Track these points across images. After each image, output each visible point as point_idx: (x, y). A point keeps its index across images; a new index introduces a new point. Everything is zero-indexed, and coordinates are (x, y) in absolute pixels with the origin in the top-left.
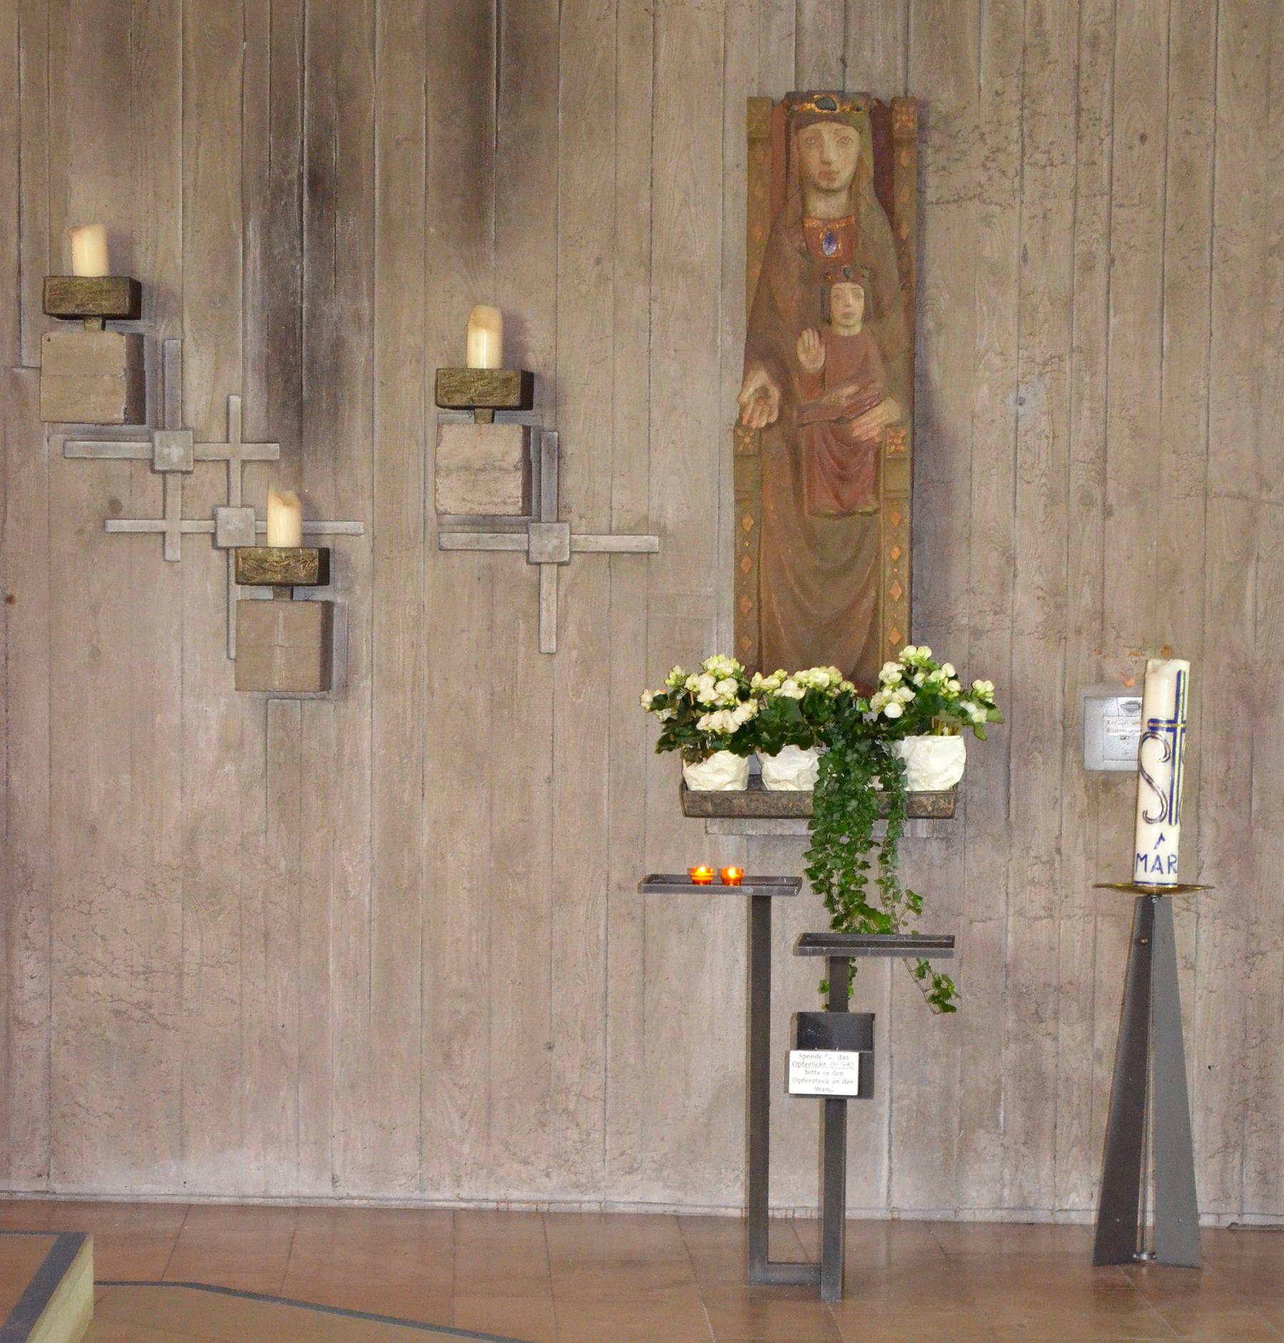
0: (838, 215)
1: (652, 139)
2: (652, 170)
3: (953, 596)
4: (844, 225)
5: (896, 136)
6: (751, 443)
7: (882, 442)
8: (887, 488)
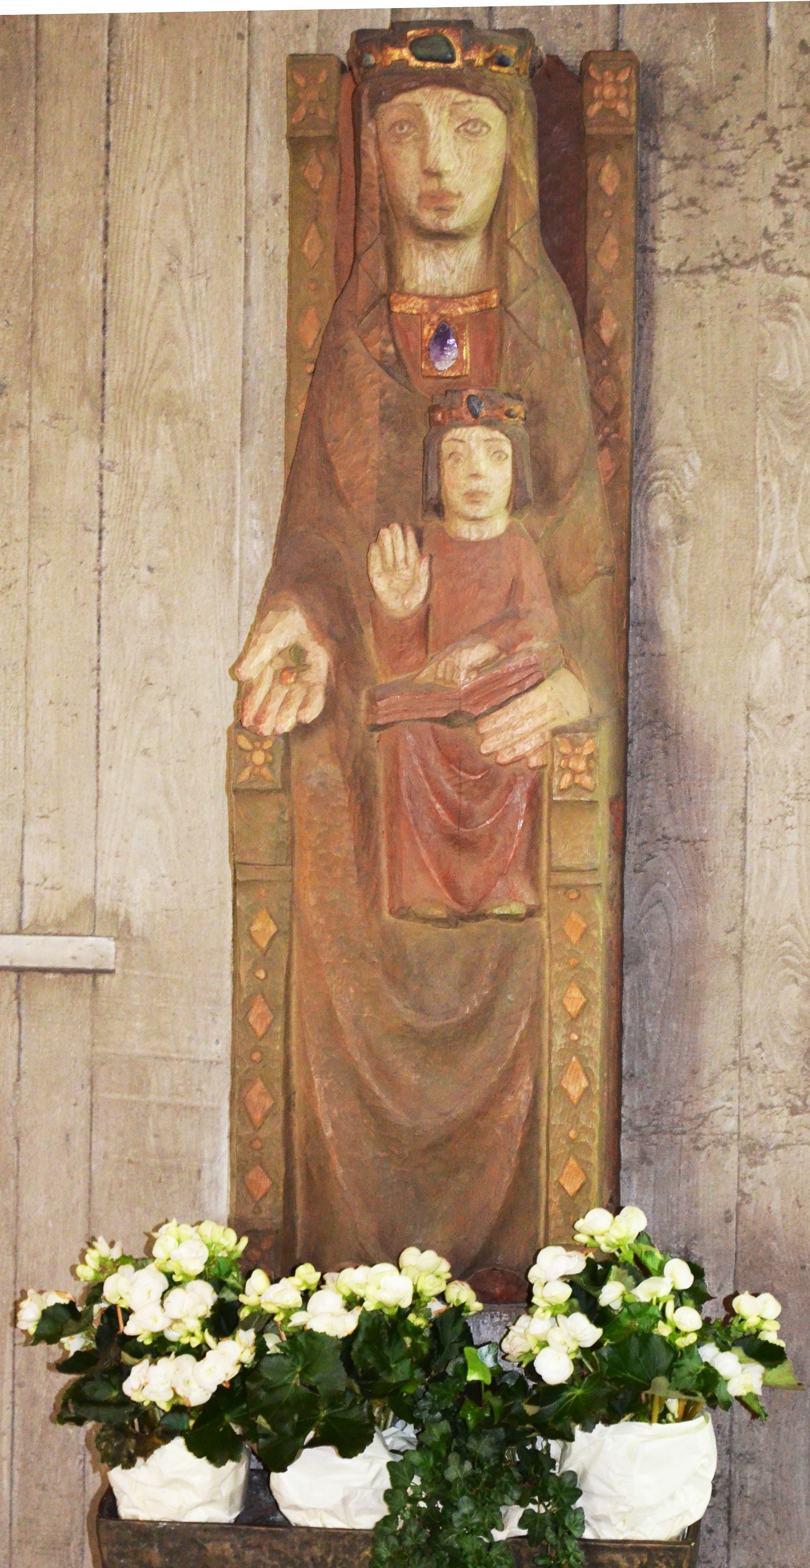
0: (462, 288)
1: (108, 146)
2: (107, 208)
3: (706, 1074)
4: (474, 308)
5: (592, 130)
6: (269, 764)
7: (544, 766)
8: (554, 864)
